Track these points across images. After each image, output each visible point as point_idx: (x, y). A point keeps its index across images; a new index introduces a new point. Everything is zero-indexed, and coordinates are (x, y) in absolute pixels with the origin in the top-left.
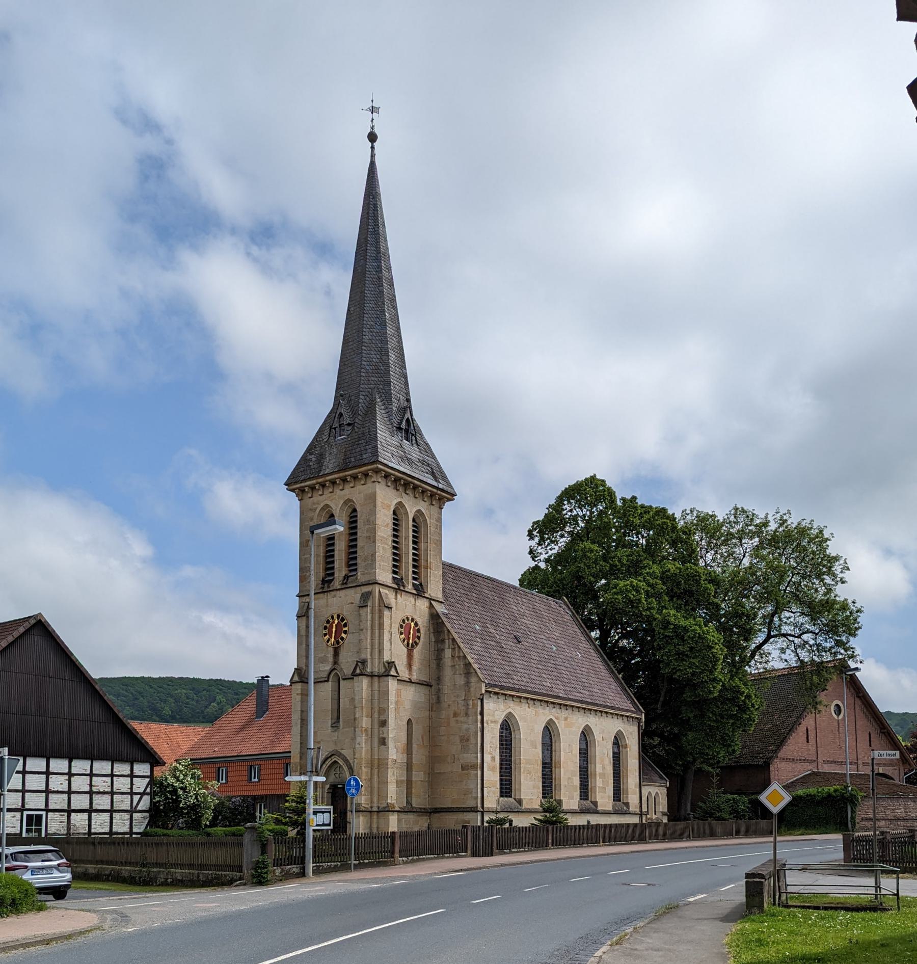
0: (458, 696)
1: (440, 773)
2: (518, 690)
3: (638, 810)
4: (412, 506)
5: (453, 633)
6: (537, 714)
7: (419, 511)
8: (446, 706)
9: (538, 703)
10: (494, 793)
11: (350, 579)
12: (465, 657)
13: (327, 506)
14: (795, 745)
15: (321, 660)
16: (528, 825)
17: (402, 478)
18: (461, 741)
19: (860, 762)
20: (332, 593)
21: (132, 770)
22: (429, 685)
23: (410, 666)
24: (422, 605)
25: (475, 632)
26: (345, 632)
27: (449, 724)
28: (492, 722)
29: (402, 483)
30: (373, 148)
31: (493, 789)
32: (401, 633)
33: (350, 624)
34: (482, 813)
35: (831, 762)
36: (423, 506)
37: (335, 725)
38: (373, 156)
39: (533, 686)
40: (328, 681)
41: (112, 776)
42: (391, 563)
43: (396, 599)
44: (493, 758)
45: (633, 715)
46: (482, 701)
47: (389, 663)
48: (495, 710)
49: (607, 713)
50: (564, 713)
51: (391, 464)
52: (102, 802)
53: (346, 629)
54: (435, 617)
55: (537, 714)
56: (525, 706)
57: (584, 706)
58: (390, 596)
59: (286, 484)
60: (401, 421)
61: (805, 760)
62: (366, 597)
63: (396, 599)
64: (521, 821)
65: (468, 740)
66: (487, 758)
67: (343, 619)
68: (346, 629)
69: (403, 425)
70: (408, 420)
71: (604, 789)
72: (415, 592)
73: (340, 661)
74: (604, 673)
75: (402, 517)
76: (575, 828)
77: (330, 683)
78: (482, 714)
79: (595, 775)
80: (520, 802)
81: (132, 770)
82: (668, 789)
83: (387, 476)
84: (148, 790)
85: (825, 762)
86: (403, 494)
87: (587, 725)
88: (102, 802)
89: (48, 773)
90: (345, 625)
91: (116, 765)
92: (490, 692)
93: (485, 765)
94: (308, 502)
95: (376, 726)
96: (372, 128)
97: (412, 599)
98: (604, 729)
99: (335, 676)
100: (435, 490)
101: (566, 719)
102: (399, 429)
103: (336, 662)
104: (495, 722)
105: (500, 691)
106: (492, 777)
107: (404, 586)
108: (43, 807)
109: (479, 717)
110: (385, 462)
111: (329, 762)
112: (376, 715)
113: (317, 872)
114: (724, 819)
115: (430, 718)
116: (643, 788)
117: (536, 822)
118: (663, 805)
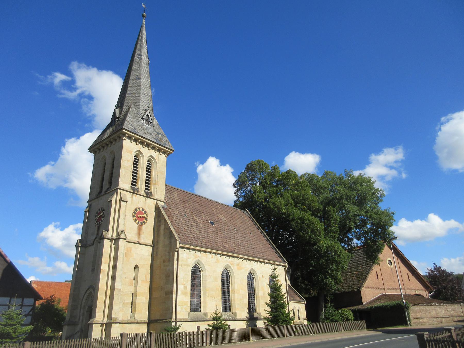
6: (218, 261)
7: (152, 156)
10: (186, 309)
14: (371, 280)
17: (139, 139)
19: (406, 288)
21: (22, 302)
23: (139, 234)
28: (185, 265)
31: (185, 307)
35: (391, 289)
36: (153, 153)
40: (93, 245)
44: (185, 287)
55: (218, 261)
57: (249, 258)
58: (128, 196)
61: (378, 288)
64: (234, 325)
71: (454, 310)
72: (146, 195)
76: (235, 331)
79: (259, 297)
81: (22, 302)
82: (306, 305)
84: (31, 313)
85: (388, 289)
87: (252, 269)
101: (238, 265)
104: (188, 265)
108: (178, 317)
111: (88, 293)
114: (336, 321)
117: (209, 327)
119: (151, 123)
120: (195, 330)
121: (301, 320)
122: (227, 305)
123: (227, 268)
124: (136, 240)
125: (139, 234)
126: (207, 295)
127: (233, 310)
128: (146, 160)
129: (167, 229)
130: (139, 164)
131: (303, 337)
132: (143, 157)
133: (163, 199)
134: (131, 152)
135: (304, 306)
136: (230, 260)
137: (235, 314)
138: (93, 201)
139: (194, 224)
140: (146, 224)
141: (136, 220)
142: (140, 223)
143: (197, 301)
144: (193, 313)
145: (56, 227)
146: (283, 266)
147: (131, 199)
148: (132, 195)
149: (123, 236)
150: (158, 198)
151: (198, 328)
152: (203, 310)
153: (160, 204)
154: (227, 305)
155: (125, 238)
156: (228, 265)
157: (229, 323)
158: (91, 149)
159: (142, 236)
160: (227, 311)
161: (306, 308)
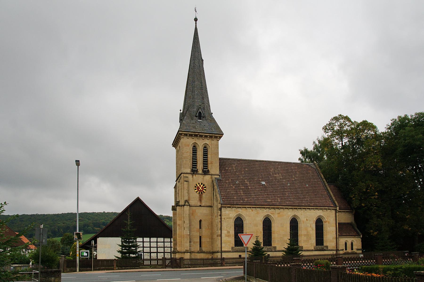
16: (114, 258)
22: (211, 207)
23: (200, 200)
24: (208, 177)
28: (227, 218)
30: (196, 23)
32: (196, 189)
36: (207, 141)
41: (164, 242)
48: (230, 214)
52: (161, 250)
66: (224, 232)
69: (197, 115)
76: (273, 257)
78: (221, 215)
82: (362, 238)
83: (186, 135)
88: (153, 250)
89: (143, 242)
91: (165, 239)
97: (201, 176)
101: (279, 213)
109: (219, 217)
113: (80, 271)
125: (200, 200)
127: (273, 245)
132: (199, 146)
135: (360, 239)
136: (270, 211)
137: (275, 248)
141: (197, 192)
145: (371, 127)
147: (192, 178)
148: (193, 176)
150: (213, 173)
157: (269, 253)
159: (203, 201)
161: (93, 213)
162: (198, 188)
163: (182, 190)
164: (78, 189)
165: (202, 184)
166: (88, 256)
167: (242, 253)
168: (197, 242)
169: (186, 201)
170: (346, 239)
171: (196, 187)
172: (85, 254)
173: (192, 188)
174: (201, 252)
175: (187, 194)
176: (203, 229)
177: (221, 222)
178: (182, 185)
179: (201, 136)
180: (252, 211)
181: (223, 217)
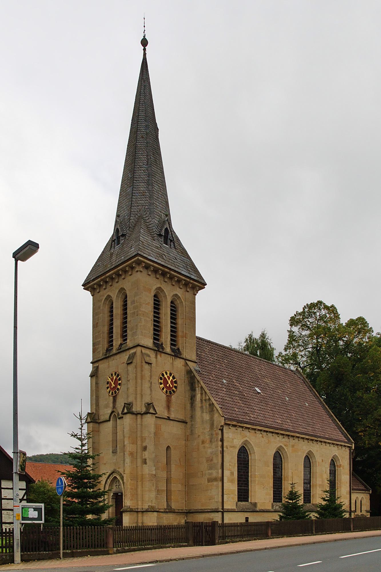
0: (204, 429)
1: (193, 485)
2: (253, 424)
3: (348, 509)
4: (170, 291)
5: (202, 383)
7: (176, 295)
8: (197, 436)
9: (270, 435)
10: (233, 498)
11: (123, 346)
12: (209, 399)
13: (109, 296)
15: (107, 406)
18: (207, 461)
20: (112, 358)
22: (185, 422)
23: (168, 407)
24: (179, 363)
25: (223, 384)
26: (120, 384)
27: (198, 449)
28: (231, 447)
29: (162, 273)
30: (145, 50)
31: (232, 496)
32: (161, 384)
33: (123, 379)
34: (223, 513)
36: (179, 292)
37: (114, 452)
38: (145, 54)
39: (266, 422)
40: (109, 420)
42: (152, 332)
43: (156, 358)
44: (232, 474)
45: (346, 445)
46: (222, 430)
47: (149, 404)
48: (234, 438)
49: (325, 442)
50: (292, 441)
51: (149, 257)
53: (119, 382)
54: (189, 372)
56: (259, 434)
57: (307, 437)
59: (83, 285)
60: (161, 230)
62: (132, 357)
63: (156, 358)
65: (212, 460)
66: (227, 473)
67: (118, 375)
68: (119, 382)
69: (163, 233)
70: (166, 229)
73: (116, 406)
74: (326, 417)
75: (161, 298)
77: (111, 421)
78: (222, 440)
79: (316, 485)
80: (255, 505)
82: (371, 495)
83: (147, 267)
84: (25, 498)
86: (163, 282)
90: (120, 379)
92: (229, 425)
93: (225, 478)
94: (97, 295)
95: (139, 450)
96: (144, 37)
97: (169, 359)
98: (323, 454)
99: (115, 416)
100: (188, 280)
101: (293, 446)
102: (160, 235)
103: (114, 407)
104: (234, 447)
105: (236, 423)
106: (232, 487)
107: (163, 348)
109: (220, 443)
110: (145, 255)
111: (111, 478)
112: (139, 443)
113: (24, 560)
115: (186, 446)
116: (352, 495)
118: (366, 505)
119: (171, 241)
120: (244, 521)
121: (364, 513)
122: (278, 494)
123: (279, 449)
124: (166, 415)
126: (257, 482)
128: (169, 300)
129: (205, 400)
130: (160, 307)
131: (105, 556)
132: (165, 296)
133: (194, 358)
134: (149, 290)
135: (368, 496)
136: (284, 440)
138: (100, 362)
139: (236, 392)
140: (175, 394)
142: (168, 392)
143: (244, 489)
144: (240, 502)
146: (348, 447)
147: (155, 359)
148: (156, 355)
149: (151, 411)
150: (188, 357)
151: (247, 519)
152: (251, 500)
153: (191, 365)
154: (278, 494)
155: (154, 412)
156: (281, 446)
158: (86, 285)
159: (172, 409)
160: (278, 502)
162: (166, 382)
163: (139, 381)
164: (15, 327)
165: (171, 374)
166: (39, 518)
167: (249, 513)
168: (163, 491)
169: (149, 405)
170: (357, 496)
171: (161, 379)
172: (33, 514)
173: (156, 380)
174: (169, 510)
175: (148, 392)
176: (173, 467)
177: (222, 452)
178: (139, 369)
179: (171, 278)
180: (263, 437)
181: (225, 444)
